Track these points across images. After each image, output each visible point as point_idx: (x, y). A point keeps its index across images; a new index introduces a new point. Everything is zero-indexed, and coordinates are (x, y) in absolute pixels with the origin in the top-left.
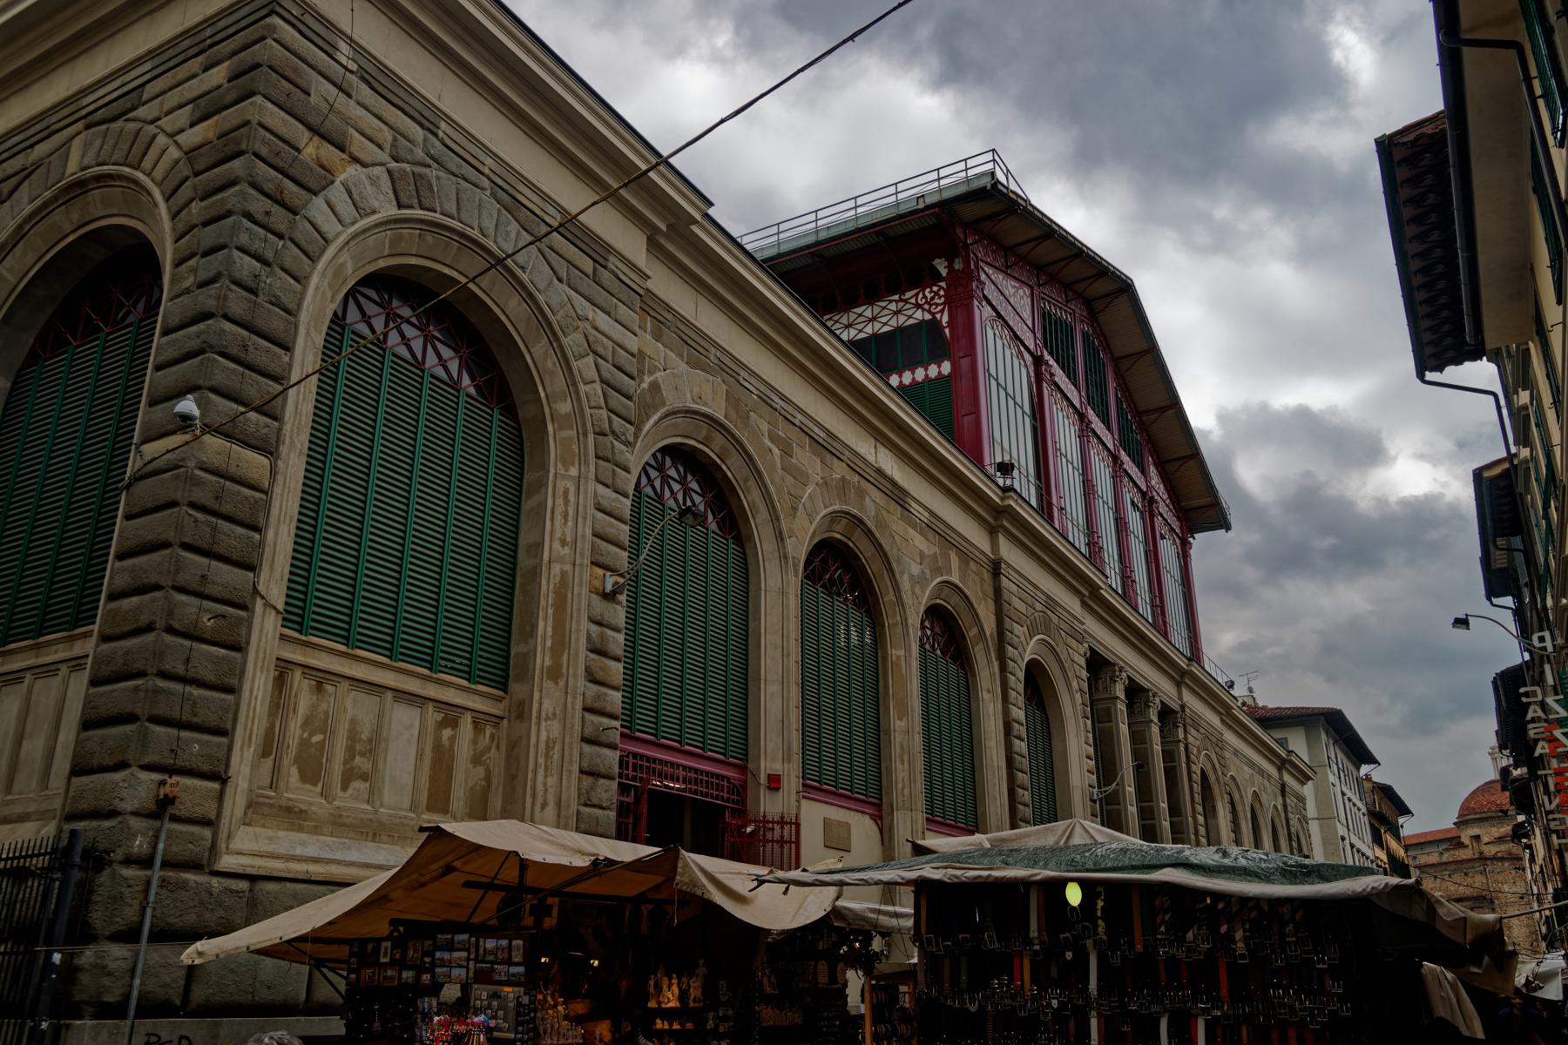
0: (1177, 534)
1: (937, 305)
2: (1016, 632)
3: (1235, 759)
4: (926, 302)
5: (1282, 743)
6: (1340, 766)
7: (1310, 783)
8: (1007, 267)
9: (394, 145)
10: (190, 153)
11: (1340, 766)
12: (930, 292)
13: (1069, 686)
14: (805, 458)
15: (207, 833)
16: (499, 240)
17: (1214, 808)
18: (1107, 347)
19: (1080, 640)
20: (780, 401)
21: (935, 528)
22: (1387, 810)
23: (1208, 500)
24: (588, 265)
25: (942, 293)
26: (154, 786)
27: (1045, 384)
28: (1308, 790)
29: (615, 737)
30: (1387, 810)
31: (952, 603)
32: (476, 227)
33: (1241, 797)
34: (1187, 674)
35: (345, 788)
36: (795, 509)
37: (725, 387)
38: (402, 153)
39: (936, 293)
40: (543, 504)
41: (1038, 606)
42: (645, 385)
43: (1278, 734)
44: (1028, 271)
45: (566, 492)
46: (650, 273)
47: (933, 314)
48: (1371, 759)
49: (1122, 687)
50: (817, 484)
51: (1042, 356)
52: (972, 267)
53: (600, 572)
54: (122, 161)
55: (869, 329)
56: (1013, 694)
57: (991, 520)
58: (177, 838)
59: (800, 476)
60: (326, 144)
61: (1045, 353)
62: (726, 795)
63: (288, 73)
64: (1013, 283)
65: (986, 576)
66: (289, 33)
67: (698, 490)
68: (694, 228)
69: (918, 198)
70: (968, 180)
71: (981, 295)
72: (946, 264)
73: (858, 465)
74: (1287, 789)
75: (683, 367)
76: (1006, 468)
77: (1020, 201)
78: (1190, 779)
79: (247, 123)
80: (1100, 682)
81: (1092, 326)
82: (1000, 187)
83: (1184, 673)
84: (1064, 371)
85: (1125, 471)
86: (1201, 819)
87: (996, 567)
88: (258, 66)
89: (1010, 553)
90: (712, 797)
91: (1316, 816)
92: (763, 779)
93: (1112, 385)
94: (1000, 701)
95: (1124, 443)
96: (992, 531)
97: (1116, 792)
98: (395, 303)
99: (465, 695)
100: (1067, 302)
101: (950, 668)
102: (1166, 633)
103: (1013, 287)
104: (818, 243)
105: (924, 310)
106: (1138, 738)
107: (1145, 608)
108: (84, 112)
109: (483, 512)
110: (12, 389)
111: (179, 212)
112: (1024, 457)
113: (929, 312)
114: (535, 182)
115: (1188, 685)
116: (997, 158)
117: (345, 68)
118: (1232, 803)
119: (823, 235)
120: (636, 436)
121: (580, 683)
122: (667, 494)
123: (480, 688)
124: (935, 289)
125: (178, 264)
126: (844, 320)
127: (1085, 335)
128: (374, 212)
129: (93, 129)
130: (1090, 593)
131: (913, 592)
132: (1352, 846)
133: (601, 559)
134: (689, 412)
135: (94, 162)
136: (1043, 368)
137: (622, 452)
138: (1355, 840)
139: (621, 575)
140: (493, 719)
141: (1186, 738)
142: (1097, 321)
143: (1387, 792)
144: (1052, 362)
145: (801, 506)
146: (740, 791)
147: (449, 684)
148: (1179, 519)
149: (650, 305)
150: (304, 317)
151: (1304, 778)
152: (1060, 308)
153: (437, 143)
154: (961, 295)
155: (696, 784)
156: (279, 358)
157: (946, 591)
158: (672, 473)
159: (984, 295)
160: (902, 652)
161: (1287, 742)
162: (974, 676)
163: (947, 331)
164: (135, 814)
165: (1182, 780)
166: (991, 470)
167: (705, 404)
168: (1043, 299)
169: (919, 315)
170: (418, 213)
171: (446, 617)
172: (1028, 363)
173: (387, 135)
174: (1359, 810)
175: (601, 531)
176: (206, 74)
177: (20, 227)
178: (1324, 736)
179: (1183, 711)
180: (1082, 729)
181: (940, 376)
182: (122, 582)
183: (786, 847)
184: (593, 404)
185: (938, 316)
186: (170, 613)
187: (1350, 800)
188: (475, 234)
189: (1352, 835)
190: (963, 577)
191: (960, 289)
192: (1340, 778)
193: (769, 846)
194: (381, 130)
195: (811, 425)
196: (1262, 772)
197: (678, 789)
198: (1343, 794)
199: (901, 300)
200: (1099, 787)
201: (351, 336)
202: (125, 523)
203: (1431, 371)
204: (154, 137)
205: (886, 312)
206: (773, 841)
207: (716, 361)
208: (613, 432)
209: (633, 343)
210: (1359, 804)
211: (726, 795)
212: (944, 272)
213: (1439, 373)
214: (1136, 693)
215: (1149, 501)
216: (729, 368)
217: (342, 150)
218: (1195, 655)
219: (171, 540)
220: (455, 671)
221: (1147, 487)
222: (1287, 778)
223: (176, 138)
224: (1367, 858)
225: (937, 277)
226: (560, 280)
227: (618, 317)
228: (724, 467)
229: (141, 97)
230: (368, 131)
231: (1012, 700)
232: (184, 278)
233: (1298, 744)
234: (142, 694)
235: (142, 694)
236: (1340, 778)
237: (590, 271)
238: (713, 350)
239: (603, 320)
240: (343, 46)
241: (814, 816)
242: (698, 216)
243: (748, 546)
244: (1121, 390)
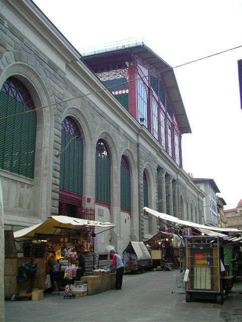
9: (15, 46)
21: (126, 136)
22: (220, 204)
24: (53, 72)
28: (204, 200)
30: (220, 204)
31: (128, 154)
34: (179, 170)
36: (95, 132)
43: (198, 185)
48: (218, 191)
55: (107, 79)
65: (136, 147)
76: (142, 120)
83: (178, 171)
87: (138, 145)
89: (141, 141)
92: (86, 199)
95: (168, 110)
96: (138, 135)
104: (95, 55)
106: (167, 187)
107: (170, 154)
112: (145, 116)
115: (142, 136)
121: (51, 178)
122: (10, 92)
123: (29, 178)
126: (100, 75)
143: (222, 200)
146: (80, 202)
147: (22, 177)
149: (66, 82)
151: (203, 196)
154: (133, 71)
158: (67, 123)
160: (116, 167)
166: (139, 121)
169: (121, 76)
170: (19, 62)
173: (13, 43)
181: (126, 94)
188: (30, 66)
190: (131, 147)
196: (194, 195)
208: (58, 115)
209: (62, 92)
212: (128, 66)
214: (167, 175)
215: (173, 125)
216: (82, 97)
218: (181, 166)
220: (24, 175)
233: (202, 187)
239: (56, 87)
241: (97, 207)
243: (83, 141)
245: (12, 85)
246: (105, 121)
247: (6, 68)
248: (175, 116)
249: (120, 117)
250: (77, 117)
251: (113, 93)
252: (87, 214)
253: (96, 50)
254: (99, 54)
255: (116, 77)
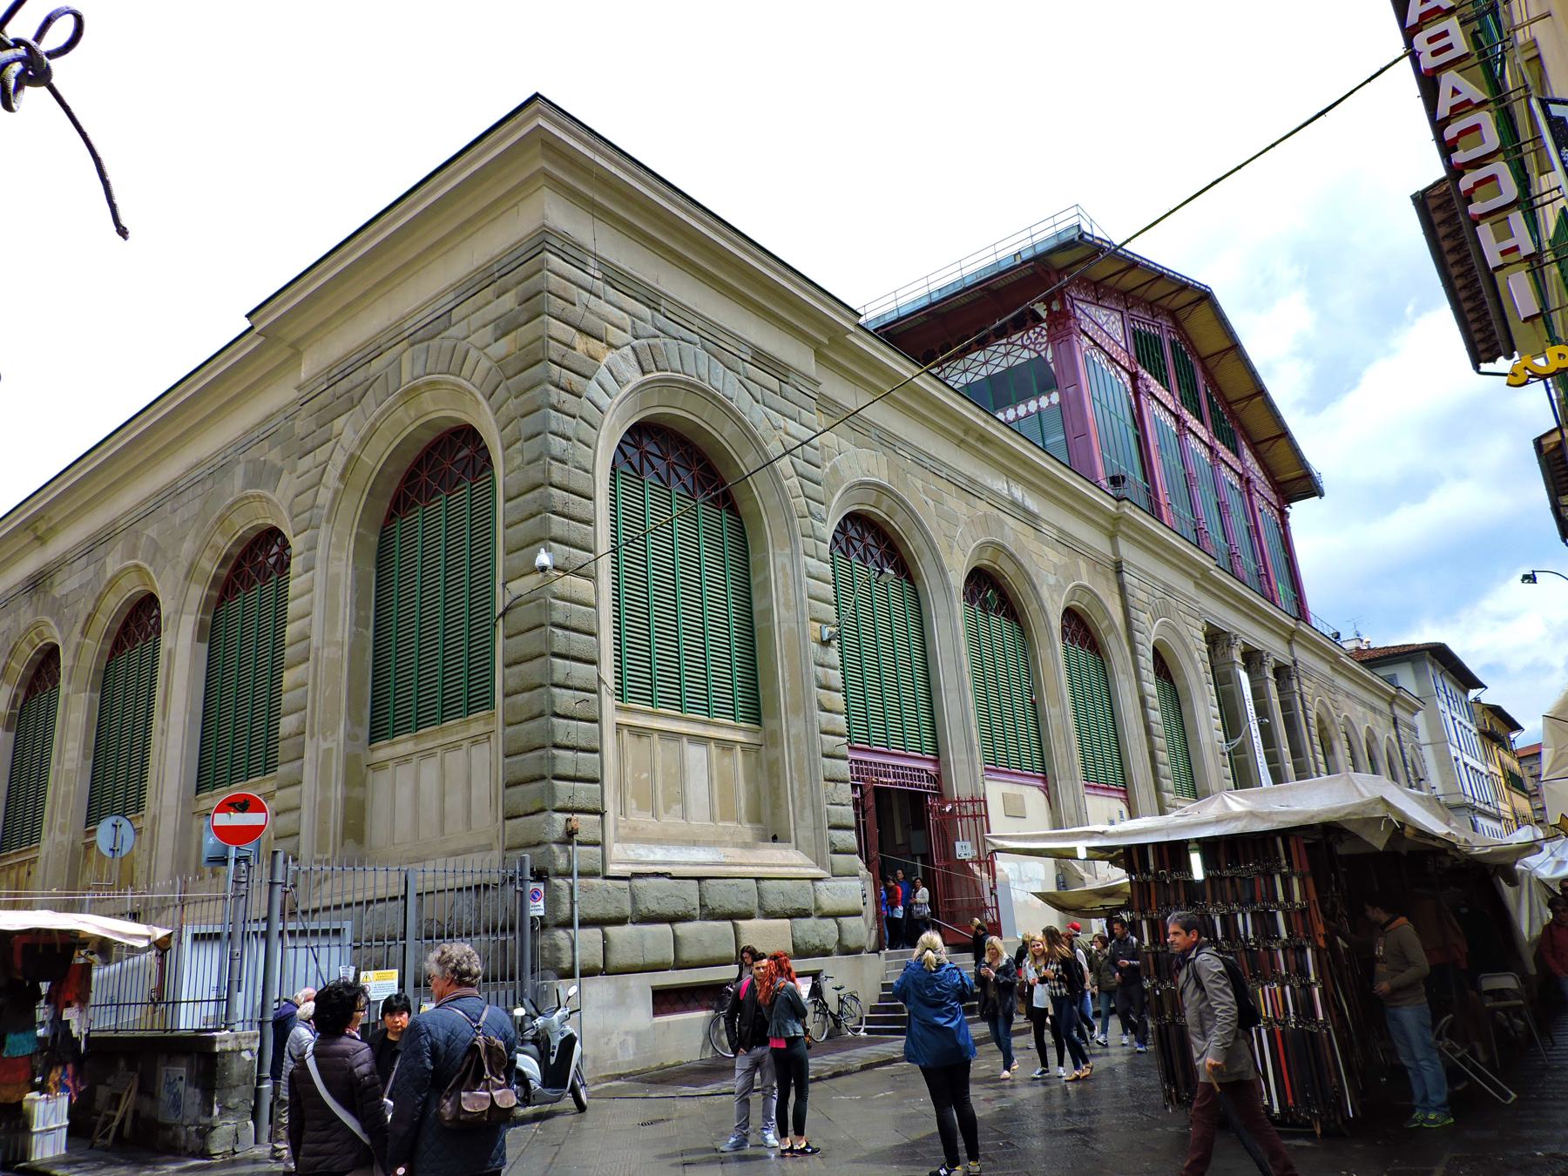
0: (1274, 507)
1: (1041, 344)
2: (1141, 619)
3: (1349, 702)
4: (1031, 342)
5: (1391, 680)
6: (1449, 694)
7: (1420, 712)
8: (1098, 299)
10: (501, 362)
11: (1449, 694)
12: (1034, 333)
13: (1191, 658)
14: (956, 504)
15: (598, 850)
16: (712, 381)
17: (1332, 748)
18: (1193, 349)
19: (1197, 617)
20: (928, 461)
22: (1499, 728)
23: (1300, 472)
24: (774, 383)
25: (1044, 333)
26: (564, 822)
27: (1142, 396)
29: (845, 750)
31: (1080, 604)
32: (695, 375)
33: (1357, 734)
35: (666, 812)
36: (951, 547)
37: (885, 458)
38: (640, 333)
39: (1039, 334)
40: (767, 579)
41: (1158, 594)
42: (827, 470)
44: (1116, 298)
45: (784, 567)
46: (819, 380)
47: (1038, 352)
48: (1479, 685)
49: (1239, 653)
50: (966, 523)
51: (1137, 372)
52: (1069, 307)
53: (818, 625)
54: (445, 371)
55: (983, 372)
56: (1144, 672)
57: (1110, 527)
58: (583, 856)
59: (952, 520)
60: (591, 339)
61: (1139, 368)
62: (926, 784)
63: (562, 293)
64: (1105, 312)
65: (1112, 575)
66: (555, 262)
67: (874, 543)
68: (850, 337)
69: (1015, 255)
70: (1058, 234)
71: (1079, 330)
72: (1045, 307)
73: (993, 498)
74: (1399, 721)
75: (852, 447)
77: (1105, 244)
78: (1309, 731)
79: (540, 337)
80: (1218, 650)
81: (1178, 334)
82: (1086, 237)
84: (1157, 380)
85: (1221, 458)
86: (1321, 758)
88: (540, 292)
89: (1128, 552)
90: (916, 786)
91: (1429, 741)
93: (1201, 383)
94: (1134, 679)
95: (1218, 433)
97: (1242, 743)
98: (645, 441)
99: (733, 732)
100: (1154, 317)
101: (1083, 655)
102: (1273, 599)
103: (1105, 315)
104: (932, 305)
105: (1030, 349)
106: (1258, 693)
108: (407, 334)
109: (725, 586)
110: (380, 542)
111: (499, 409)
113: (1034, 350)
114: (730, 329)
116: (1080, 212)
117: (594, 277)
118: (1349, 741)
119: (936, 297)
120: (828, 512)
124: (1038, 330)
125: (506, 448)
126: (961, 366)
127: (1173, 344)
128: (628, 382)
129: (416, 346)
130: (1202, 574)
131: (1052, 600)
132: (1466, 765)
133: (816, 616)
134: (862, 484)
135: (422, 373)
136: (1139, 383)
137: (820, 528)
138: (1467, 759)
139: (834, 626)
140: (754, 747)
141: (1300, 689)
142: (1182, 328)
143: (1497, 711)
144: (1146, 375)
145: (955, 544)
148: (1276, 493)
150: (598, 473)
151: (1414, 710)
152: (1148, 325)
153: (661, 317)
154: (1061, 326)
155: (903, 778)
156: (587, 506)
157: (1079, 592)
158: (853, 533)
159: (1082, 330)
161: (1396, 678)
162: (1109, 661)
163: (1052, 365)
164: (555, 842)
165: (1301, 727)
167: (874, 476)
168: (1132, 320)
169: (1026, 354)
171: (628, 647)
172: (1125, 380)
173: (627, 321)
174: (1470, 731)
175: (813, 594)
176: (499, 300)
177: (373, 425)
178: (1430, 669)
179: (1296, 665)
180: (1208, 693)
182: (513, 684)
183: (978, 820)
184: (794, 495)
185: (1043, 354)
186: (553, 703)
187: (1460, 723)
189: (1464, 754)
191: (1060, 328)
192: (1449, 704)
193: (965, 820)
194: (624, 319)
195: (954, 475)
197: (891, 784)
198: (1453, 719)
199: (1008, 343)
200: (1227, 742)
201: (622, 475)
202: (506, 641)
203: (1485, 362)
204: (467, 352)
205: (996, 355)
206: (967, 816)
207: (877, 439)
208: (811, 514)
210: (1470, 726)
211: (926, 784)
212: (1044, 315)
213: (1492, 364)
214: (1252, 658)
215: (1246, 481)
217: (601, 341)
219: (545, 651)
220: (666, 703)
221: (1243, 468)
222: (1399, 712)
223: (485, 351)
224: (1482, 774)
225: (1037, 319)
226: (757, 402)
227: (803, 422)
228: (892, 523)
229: (450, 320)
230: (615, 321)
231: (1144, 678)
232: (513, 458)
233: (1407, 678)
234: (545, 761)
235: (545, 761)
236: (1449, 704)
237: (777, 389)
238: (873, 430)
240: (591, 261)
241: (996, 792)
242: (851, 328)
243: (917, 583)
244: (1211, 386)
245: (652, 448)
246: (982, 507)
247: (616, 401)
248: (1254, 447)
249: (1135, 540)
250: (681, 409)
251: (1000, 416)
252: (961, 817)
253: (934, 287)
254: (945, 299)
255: (1011, 359)
